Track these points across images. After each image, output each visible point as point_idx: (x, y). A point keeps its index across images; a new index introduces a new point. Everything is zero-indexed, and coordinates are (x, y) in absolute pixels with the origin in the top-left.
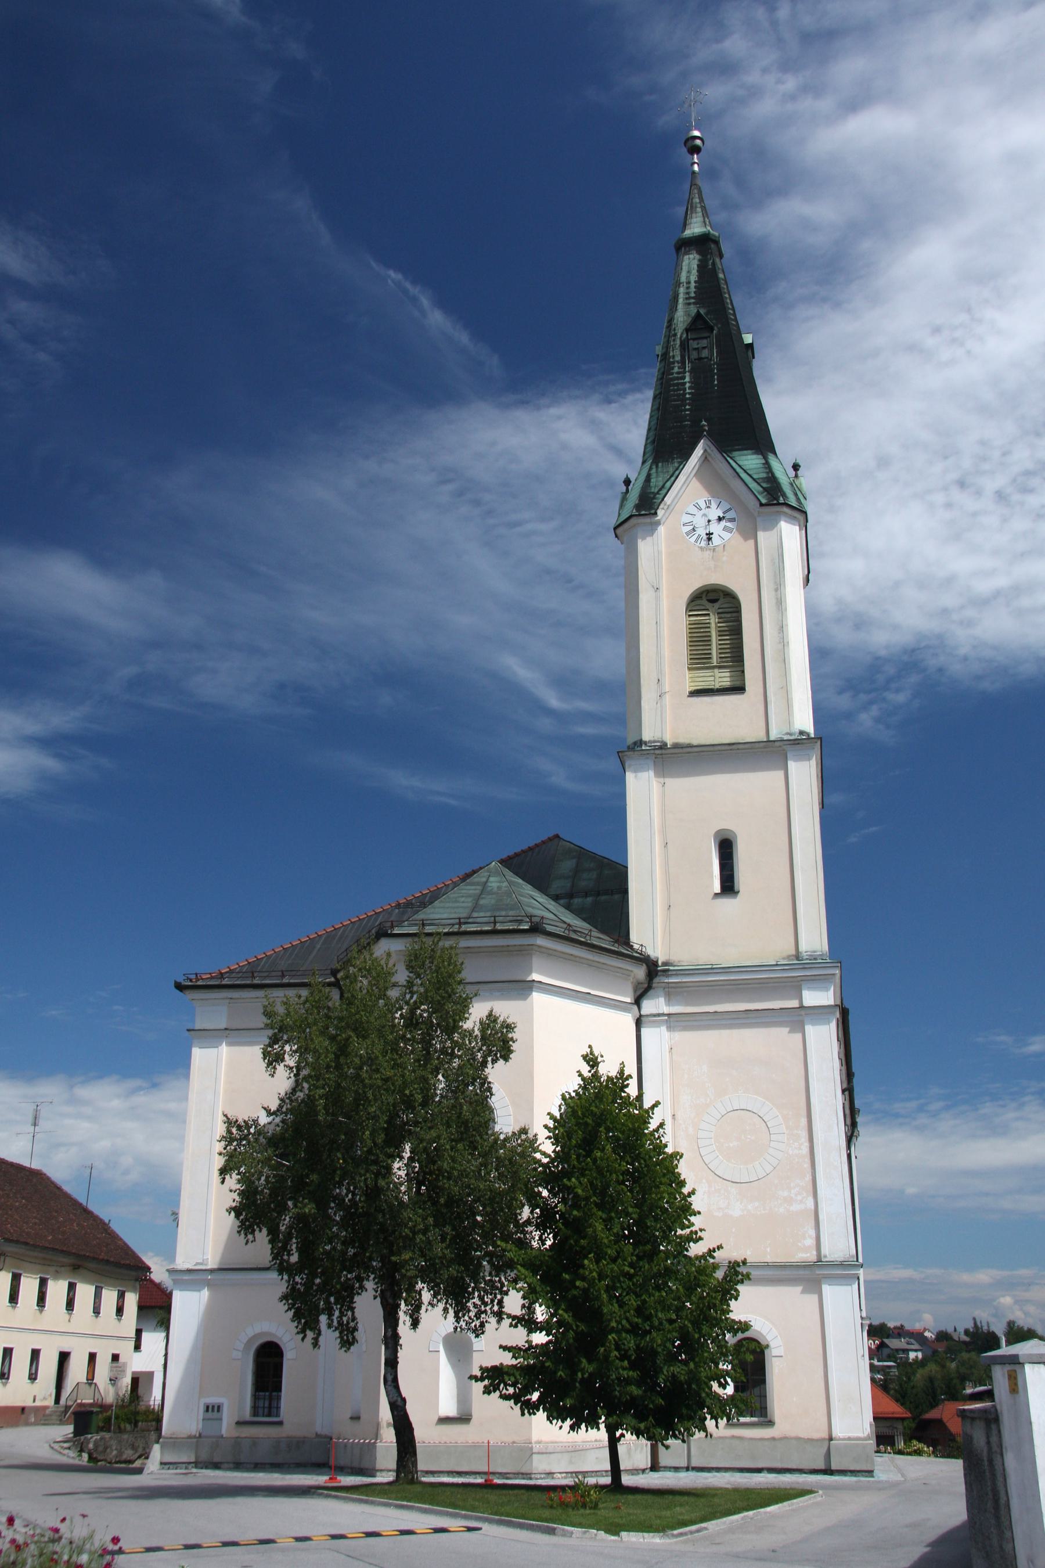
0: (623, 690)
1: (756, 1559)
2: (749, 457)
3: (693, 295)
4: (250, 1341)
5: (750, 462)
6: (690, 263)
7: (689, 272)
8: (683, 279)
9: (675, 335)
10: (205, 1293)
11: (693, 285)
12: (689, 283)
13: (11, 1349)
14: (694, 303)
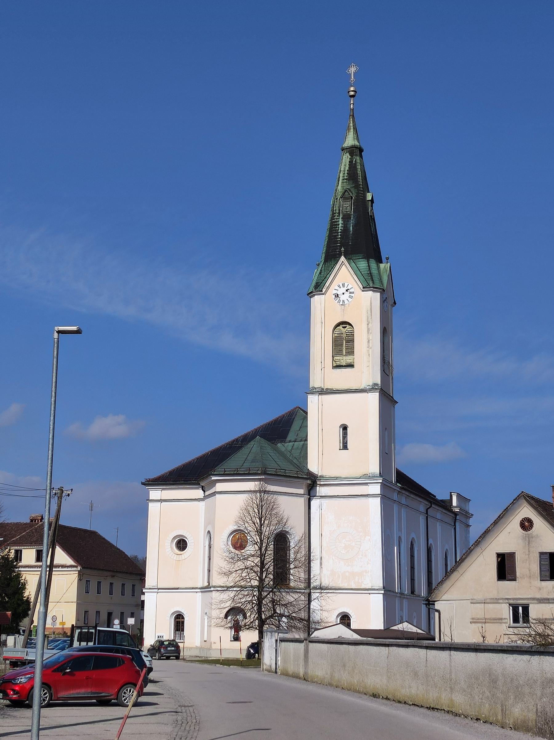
0: (303, 361)
1: (429, 708)
2: (362, 263)
3: (346, 178)
4: (173, 614)
5: (362, 265)
6: (346, 158)
7: (345, 165)
8: (342, 169)
9: (337, 199)
10: (57, 547)
11: (346, 172)
12: (344, 171)
13: (99, 612)
14: (346, 182)
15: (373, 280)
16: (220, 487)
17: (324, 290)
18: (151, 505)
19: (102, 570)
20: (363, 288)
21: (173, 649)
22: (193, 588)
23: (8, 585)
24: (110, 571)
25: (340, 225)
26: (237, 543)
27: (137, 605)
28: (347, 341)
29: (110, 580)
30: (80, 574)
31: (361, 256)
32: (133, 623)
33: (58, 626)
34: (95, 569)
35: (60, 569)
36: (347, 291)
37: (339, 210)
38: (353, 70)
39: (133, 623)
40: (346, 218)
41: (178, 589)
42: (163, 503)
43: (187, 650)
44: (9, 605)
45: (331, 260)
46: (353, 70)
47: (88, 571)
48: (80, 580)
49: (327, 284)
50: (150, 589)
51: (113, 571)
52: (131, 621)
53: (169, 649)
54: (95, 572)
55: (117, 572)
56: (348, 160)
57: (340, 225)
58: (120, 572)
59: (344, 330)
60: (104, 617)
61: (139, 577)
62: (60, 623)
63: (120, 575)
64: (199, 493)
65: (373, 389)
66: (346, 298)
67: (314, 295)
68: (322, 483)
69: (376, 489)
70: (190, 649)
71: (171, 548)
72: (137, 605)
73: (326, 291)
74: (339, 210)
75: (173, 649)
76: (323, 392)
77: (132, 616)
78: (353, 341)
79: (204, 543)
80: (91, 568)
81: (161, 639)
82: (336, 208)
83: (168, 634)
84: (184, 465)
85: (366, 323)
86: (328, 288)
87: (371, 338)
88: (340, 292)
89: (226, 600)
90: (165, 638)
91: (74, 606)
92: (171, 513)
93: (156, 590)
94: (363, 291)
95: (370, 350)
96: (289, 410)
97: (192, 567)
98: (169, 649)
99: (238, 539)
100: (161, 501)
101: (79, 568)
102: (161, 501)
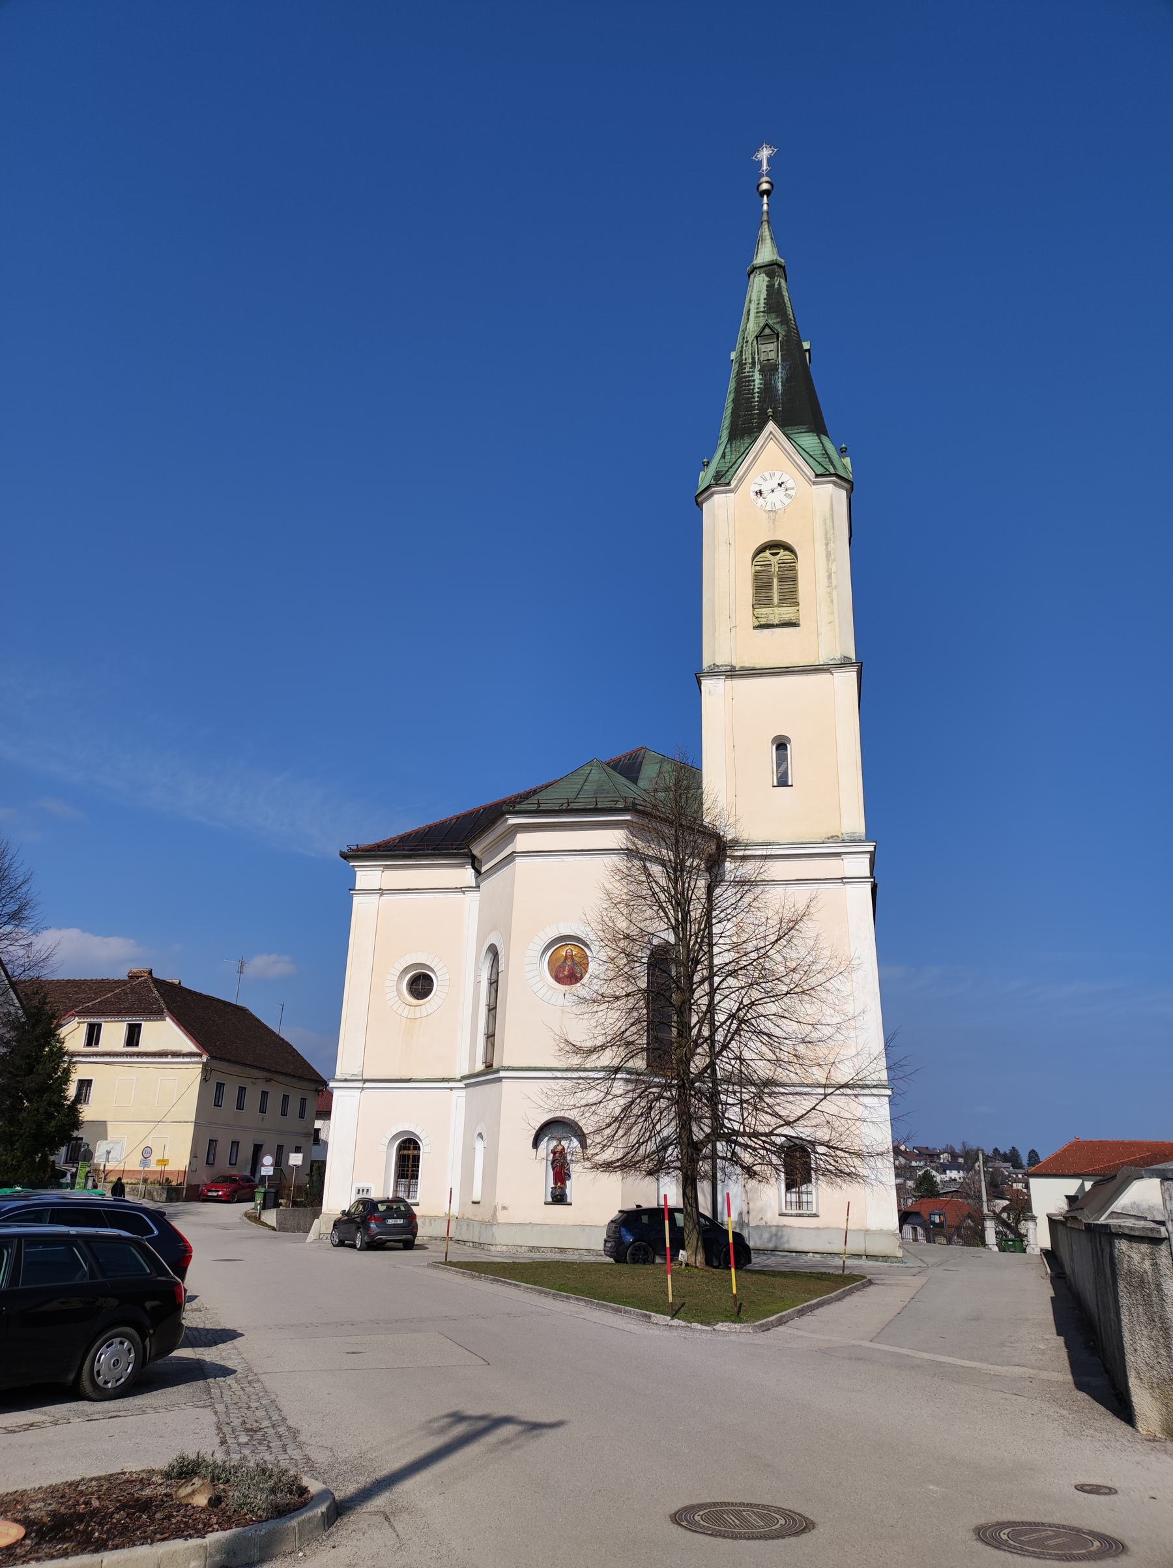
4: (395, 1137)
7: (760, 291)
8: (754, 297)
11: (762, 301)
15: (832, 464)
16: (523, 841)
17: (734, 483)
18: (357, 900)
19: (250, 1066)
20: (817, 476)
21: (400, 1221)
22: (443, 1080)
23: (30, 1070)
24: (264, 1069)
25: (757, 382)
26: (561, 968)
27: (307, 1135)
28: (782, 580)
29: (262, 1086)
30: (207, 1071)
31: (803, 428)
32: (300, 1163)
33: (153, 1167)
34: (236, 1062)
35: (170, 1059)
36: (780, 485)
37: (753, 359)
38: (765, 153)
39: (300, 1163)
40: (768, 370)
41: (409, 1081)
42: (385, 897)
43: (424, 1223)
44: (25, 1114)
45: (742, 437)
46: (765, 153)
47: (216, 1064)
48: (205, 1080)
49: (740, 472)
50: (346, 1080)
51: (269, 1071)
52: (296, 1159)
53: (390, 1222)
54: (237, 1069)
55: (276, 1072)
56: (765, 283)
57: (757, 382)
58: (283, 1074)
59: (774, 560)
60: (246, 1152)
61: (313, 1086)
62: (159, 1161)
63: (281, 1078)
64: (467, 875)
65: (844, 664)
66: (776, 500)
67: (712, 494)
68: (737, 853)
69: (860, 866)
70: (433, 1219)
71: (399, 991)
72: (307, 1135)
73: (737, 487)
74: (753, 359)
75: (400, 1221)
76: (733, 673)
77: (298, 1150)
78: (794, 579)
79: (477, 975)
80: (228, 1061)
81: (365, 1196)
82: (748, 357)
83: (382, 1187)
84: (430, 827)
85: (823, 541)
86: (741, 480)
87: (834, 569)
88: (766, 488)
89: (524, 1105)
90: (376, 1194)
91: (190, 1128)
92: (400, 914)
93: (360, 1085)
94: (814, 483)
95: (835, 593)
96: (629, 750)
97: (449, 1030)
98: (390, 1222)
99: (566, 958)
100: (382, 892)
101: (205, 1058)
102: (382, 892)
